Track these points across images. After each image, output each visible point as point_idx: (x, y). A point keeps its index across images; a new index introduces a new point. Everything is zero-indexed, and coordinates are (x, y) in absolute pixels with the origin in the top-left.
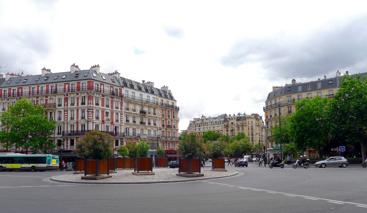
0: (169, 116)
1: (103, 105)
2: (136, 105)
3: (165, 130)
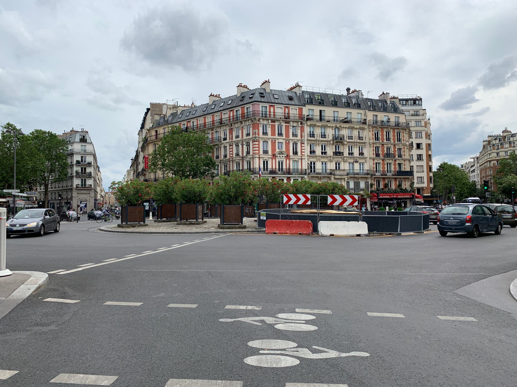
0: (388, 139)
1: (273, 134)
3: (381, 161)
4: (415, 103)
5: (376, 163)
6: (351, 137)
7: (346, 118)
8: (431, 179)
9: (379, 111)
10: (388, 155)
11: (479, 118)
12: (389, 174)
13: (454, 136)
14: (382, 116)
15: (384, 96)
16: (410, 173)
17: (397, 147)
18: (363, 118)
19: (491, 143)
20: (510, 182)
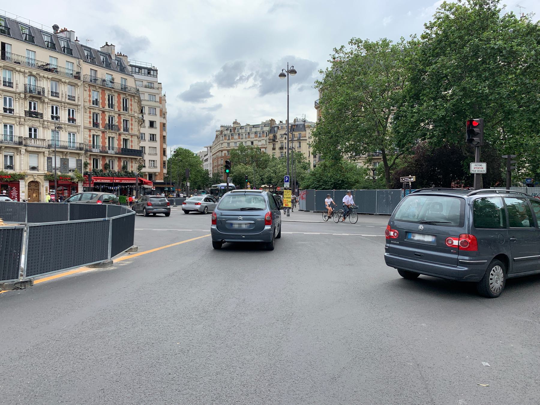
0: (111, 105)
2: (14, 75)
3: (100, 133)
4: (149, 73)
5: (94, 136)
6: (55, 94)
7: (48, 64)
8: (164, 163)
9: (100, 65)
10: (110, 126)
11: (213, 113)
12: (111, 152)
13: (192, 126)
14: (103, 73)
15: (108, 49)
16: (140, 153)
17: (123, 118)
18: (76, 69)
19: (223, 133)
20: (240, 171)
